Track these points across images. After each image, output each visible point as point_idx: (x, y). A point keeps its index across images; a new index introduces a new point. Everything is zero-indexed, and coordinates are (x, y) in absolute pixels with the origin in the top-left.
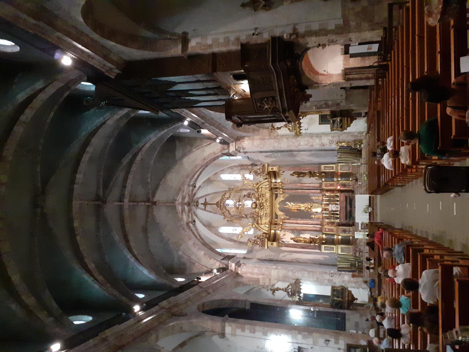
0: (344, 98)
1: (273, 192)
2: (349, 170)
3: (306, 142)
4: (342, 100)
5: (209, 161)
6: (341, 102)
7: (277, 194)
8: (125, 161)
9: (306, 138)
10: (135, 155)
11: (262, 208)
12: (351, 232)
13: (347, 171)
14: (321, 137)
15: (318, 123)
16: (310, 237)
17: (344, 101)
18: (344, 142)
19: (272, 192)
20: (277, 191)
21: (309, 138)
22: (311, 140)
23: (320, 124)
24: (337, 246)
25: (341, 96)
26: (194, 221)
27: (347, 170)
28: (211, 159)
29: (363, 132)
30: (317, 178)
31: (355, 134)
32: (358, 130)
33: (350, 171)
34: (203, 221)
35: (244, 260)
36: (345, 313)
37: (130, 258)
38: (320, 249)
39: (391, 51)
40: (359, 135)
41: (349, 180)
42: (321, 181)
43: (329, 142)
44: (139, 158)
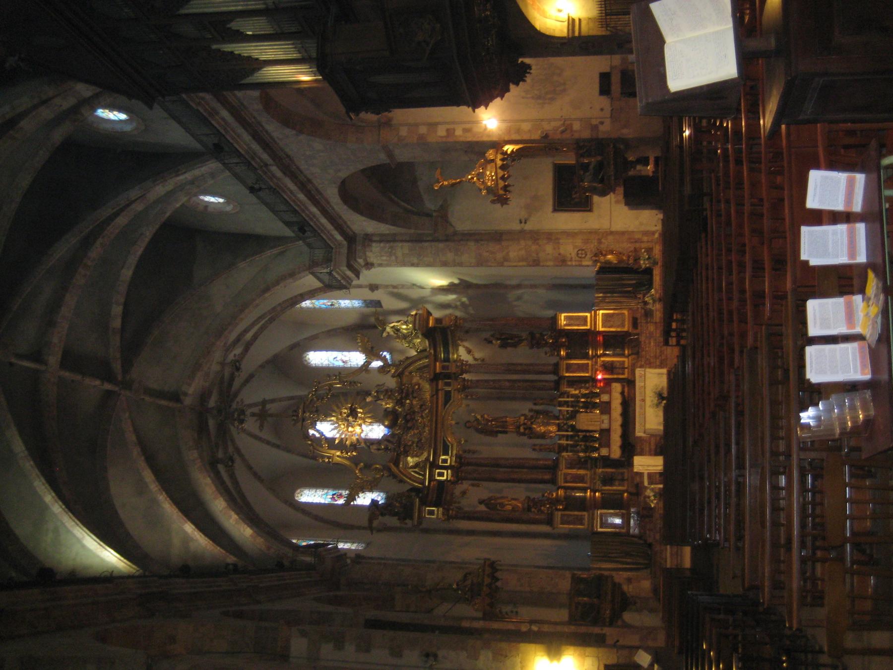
0: (609, 115)
1: (440, 387)
2: (623, 326)
3: (523, 252)
4: (602, 120)
5: (280, 304)
6: (602, 123)
7: (450, 392)
8: (62, 250)
9: (522, 243)
10: (87, 243)
11: (409, 425)
12: (626, 483)
13: (619, 330)
14: (558, 239)
15: (551, 208)
16: (528, 498)
17: (608, 122)
18: (611, 252)
19: (437, 385)
20: (448, 384)
21: (530, 243)
22: (534, 247)
23: (555, 210)
24: (591, 512)
25: (602, 110)
26: (231, 459)
27: (618, 327)
28: (284, 302)
29: (653, 233)
30: (547, 349)
31: (637, 236)
32: (642, 228)
33: (626, 329)
34: (303, 83)
35: (373, 282)
36: (604, 635)
37: (50, 504)
38: (550, 522)
39: (847, 520)
40: (645, 239)
41: (623, 355)
42: (554, 360)
43: (578, 254)
44: (95, 252)
